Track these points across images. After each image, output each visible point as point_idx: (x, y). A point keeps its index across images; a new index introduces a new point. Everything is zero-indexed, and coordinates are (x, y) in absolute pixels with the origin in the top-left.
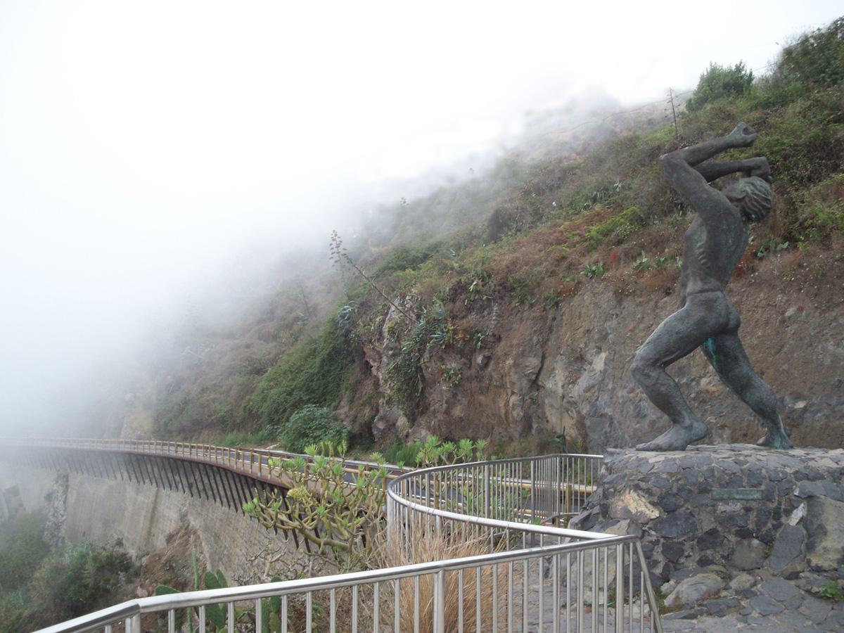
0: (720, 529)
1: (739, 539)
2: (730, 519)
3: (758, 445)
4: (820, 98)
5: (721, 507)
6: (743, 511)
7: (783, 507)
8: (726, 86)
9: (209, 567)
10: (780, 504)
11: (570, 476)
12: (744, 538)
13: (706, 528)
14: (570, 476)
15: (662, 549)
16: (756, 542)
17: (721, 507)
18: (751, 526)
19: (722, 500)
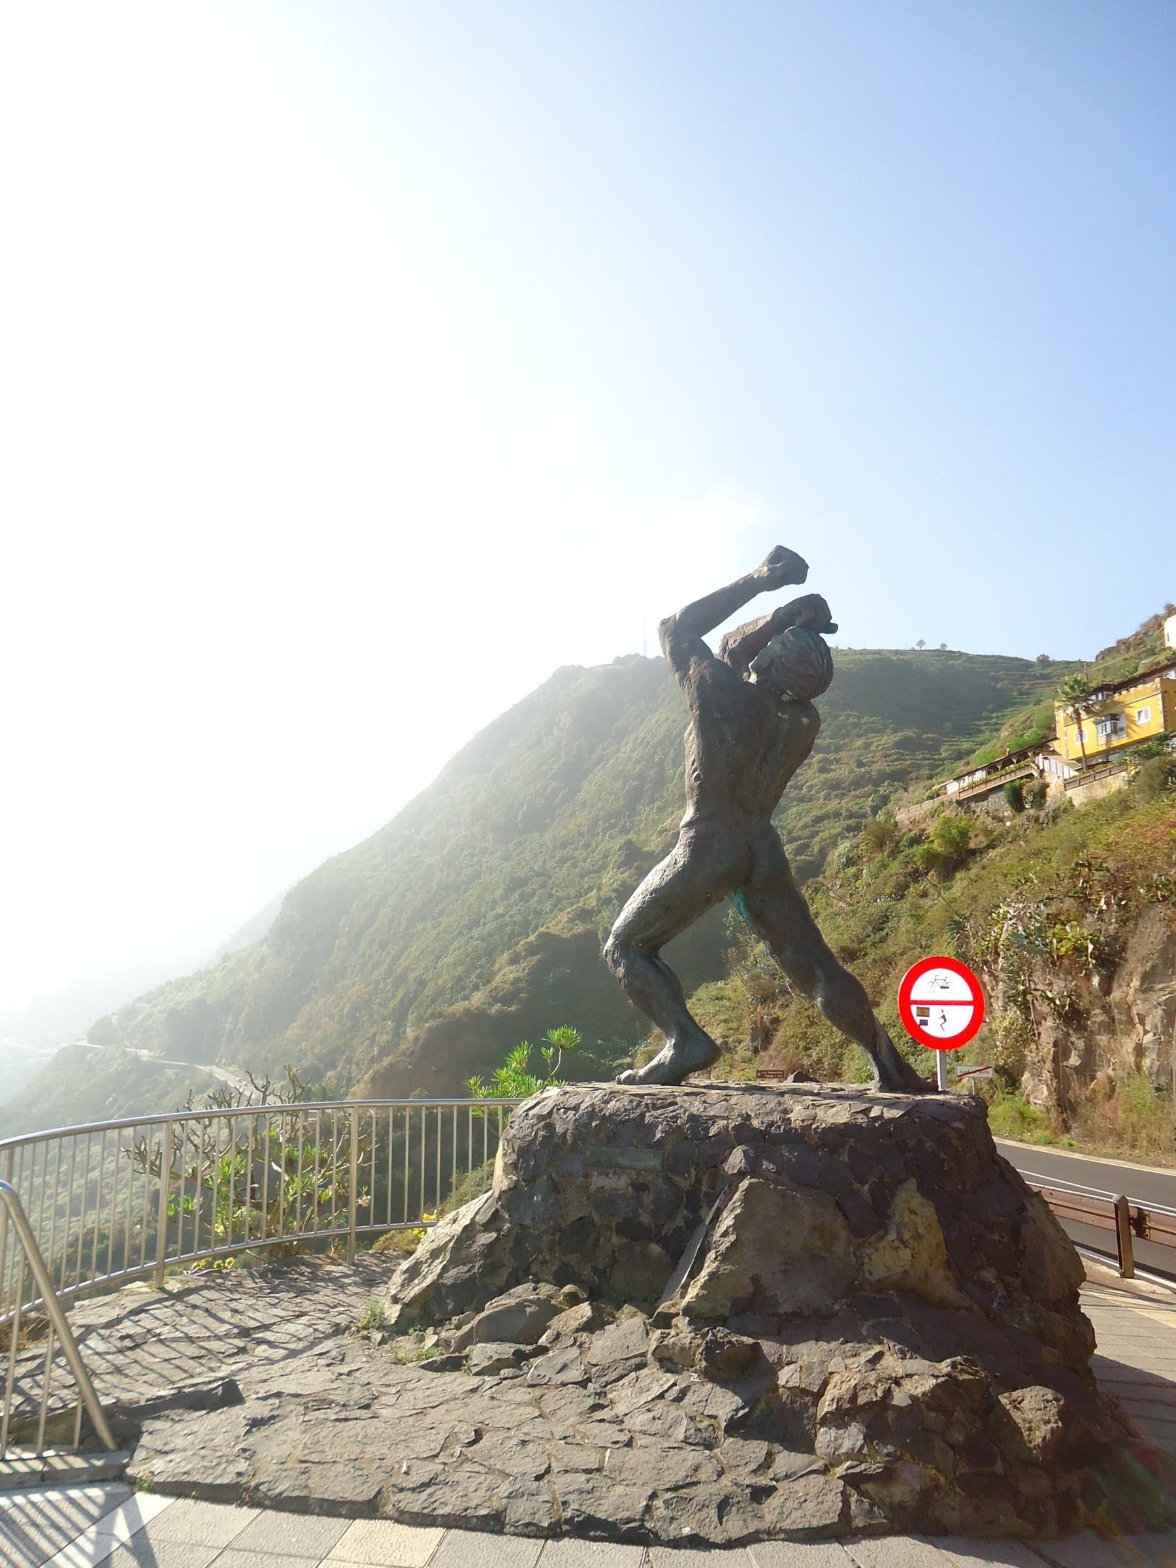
0: (596, 1218)
1: (625, 1240)
2: (605, 1201)
3: (619, 1083)
4: (33, 1315)
5: (598, 1181)
6: (630, 1189)
7: (704, 1189)
8: (581, 668)
9: (341, 924)
10: (698, 1181)
11: (431, 1129)
12: (636, 1240)
13: (574, 1216)
14: (431, 1129)
15: (512, 1244)
16: (656, 1248)
17: (598, 1181)
18: (646, 1219)
19: (597, 1165)
